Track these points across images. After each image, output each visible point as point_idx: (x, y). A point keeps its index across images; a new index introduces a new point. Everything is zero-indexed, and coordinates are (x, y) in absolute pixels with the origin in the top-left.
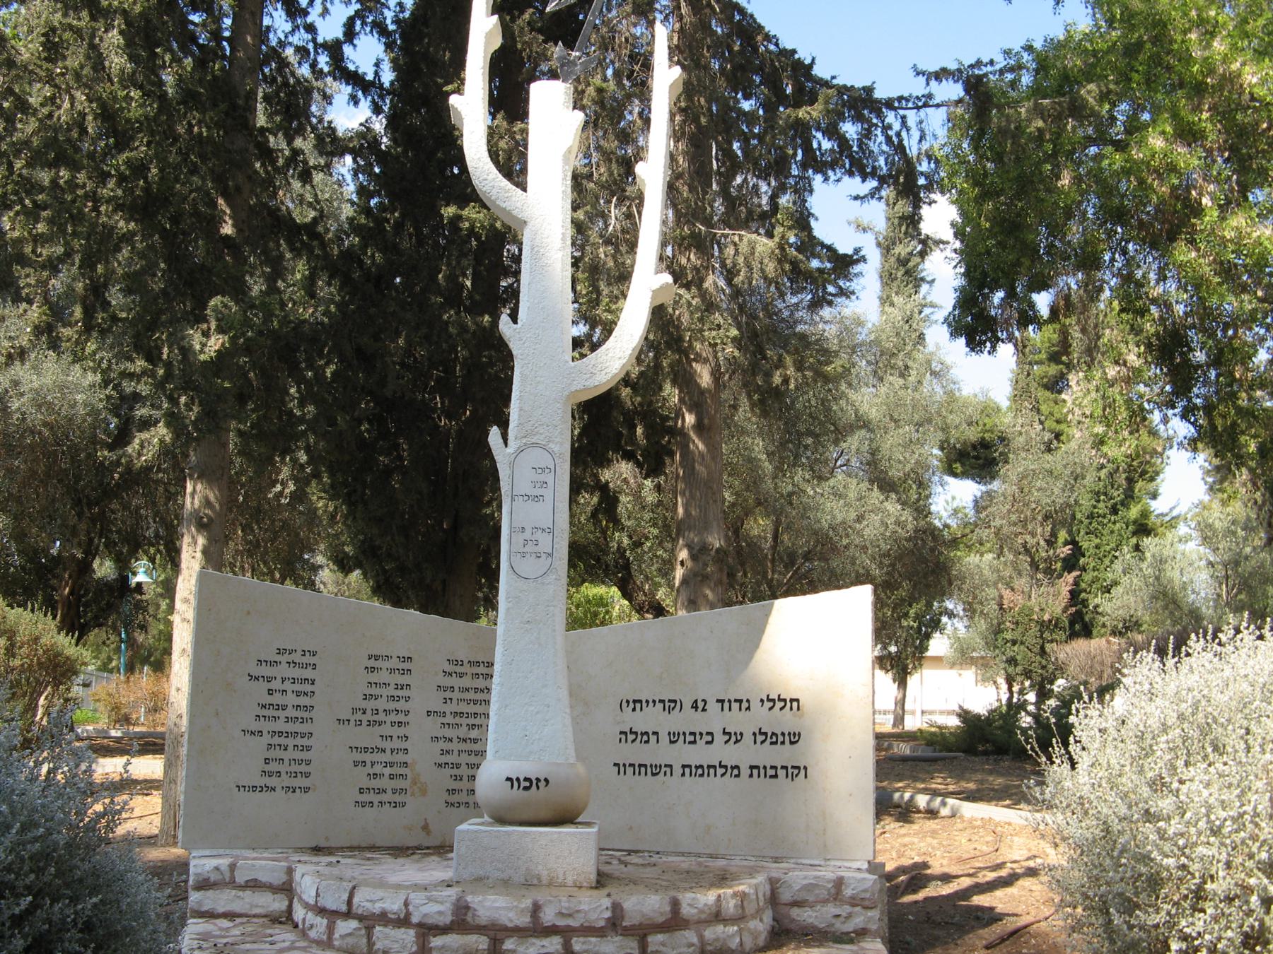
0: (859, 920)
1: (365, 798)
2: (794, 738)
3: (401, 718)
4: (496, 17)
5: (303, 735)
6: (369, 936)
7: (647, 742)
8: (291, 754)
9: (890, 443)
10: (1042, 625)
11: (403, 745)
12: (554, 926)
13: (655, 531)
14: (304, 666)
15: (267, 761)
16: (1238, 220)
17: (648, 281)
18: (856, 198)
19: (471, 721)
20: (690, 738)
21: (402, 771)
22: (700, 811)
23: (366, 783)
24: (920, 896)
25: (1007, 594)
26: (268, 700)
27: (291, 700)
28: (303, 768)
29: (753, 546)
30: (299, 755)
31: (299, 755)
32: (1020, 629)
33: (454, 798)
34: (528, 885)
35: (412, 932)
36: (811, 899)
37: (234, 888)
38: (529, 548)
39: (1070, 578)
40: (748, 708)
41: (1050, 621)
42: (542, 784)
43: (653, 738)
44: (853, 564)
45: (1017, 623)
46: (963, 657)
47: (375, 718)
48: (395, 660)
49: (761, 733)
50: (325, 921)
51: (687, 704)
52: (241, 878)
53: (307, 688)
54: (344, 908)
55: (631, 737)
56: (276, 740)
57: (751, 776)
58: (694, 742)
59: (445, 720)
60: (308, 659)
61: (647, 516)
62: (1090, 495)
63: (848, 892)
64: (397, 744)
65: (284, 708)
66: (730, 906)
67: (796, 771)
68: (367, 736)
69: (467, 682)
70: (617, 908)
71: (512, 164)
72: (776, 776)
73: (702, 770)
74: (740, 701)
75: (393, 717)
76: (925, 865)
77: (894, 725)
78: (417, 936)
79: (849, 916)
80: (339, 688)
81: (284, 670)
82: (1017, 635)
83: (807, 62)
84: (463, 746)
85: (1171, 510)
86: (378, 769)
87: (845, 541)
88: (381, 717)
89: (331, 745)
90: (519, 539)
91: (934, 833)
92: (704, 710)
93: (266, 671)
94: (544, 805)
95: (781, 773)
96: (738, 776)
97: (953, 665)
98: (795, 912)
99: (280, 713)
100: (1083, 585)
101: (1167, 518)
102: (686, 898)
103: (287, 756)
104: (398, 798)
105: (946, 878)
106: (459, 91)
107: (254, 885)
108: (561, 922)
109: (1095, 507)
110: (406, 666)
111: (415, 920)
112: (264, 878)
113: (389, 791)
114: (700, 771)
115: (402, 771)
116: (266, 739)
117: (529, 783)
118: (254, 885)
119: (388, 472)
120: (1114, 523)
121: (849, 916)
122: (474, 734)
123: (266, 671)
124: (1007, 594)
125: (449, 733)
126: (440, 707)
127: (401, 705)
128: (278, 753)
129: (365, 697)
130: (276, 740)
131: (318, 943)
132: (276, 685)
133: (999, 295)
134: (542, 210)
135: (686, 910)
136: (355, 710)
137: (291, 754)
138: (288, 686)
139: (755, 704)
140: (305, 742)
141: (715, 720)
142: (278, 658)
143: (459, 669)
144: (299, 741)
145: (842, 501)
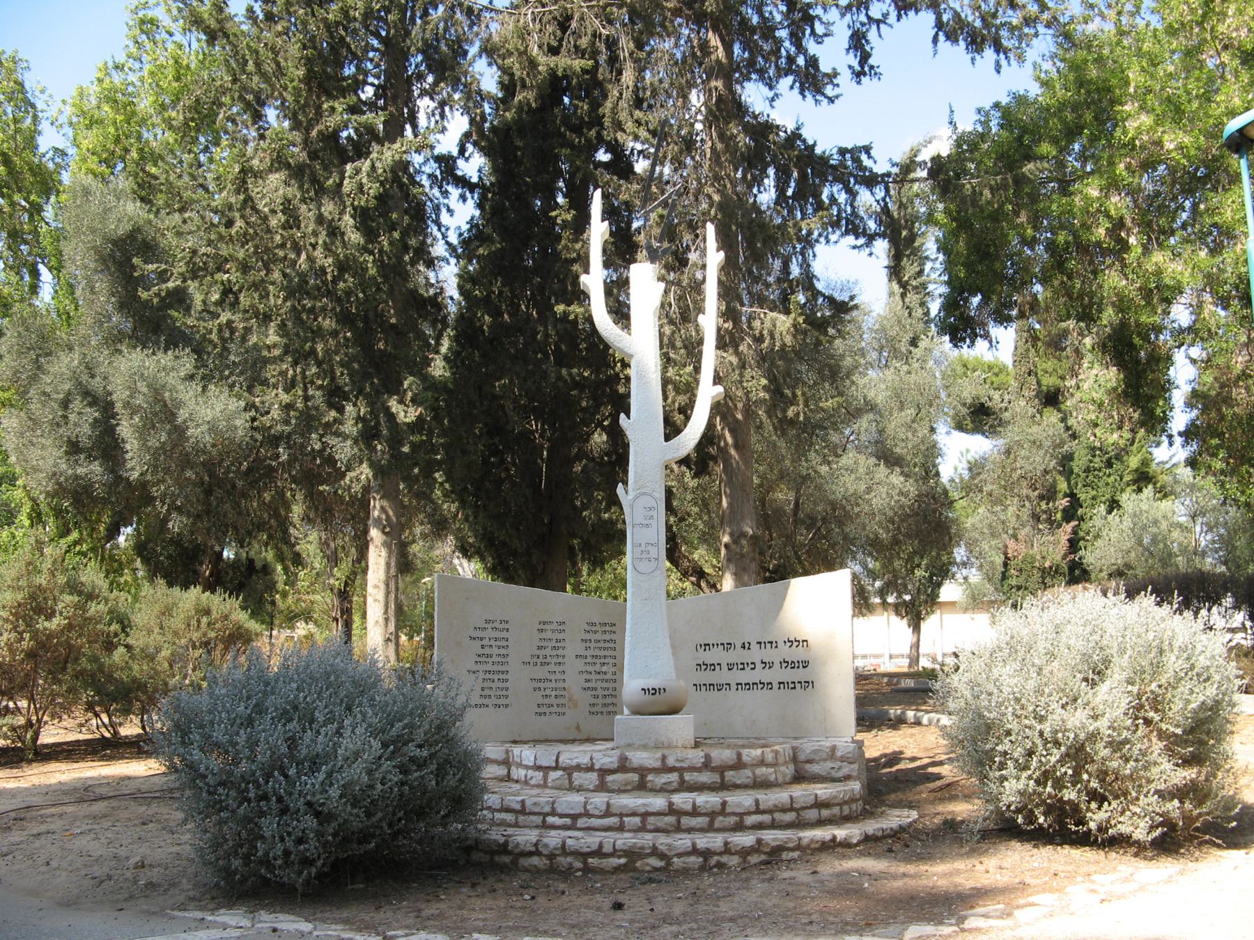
0: (846, 770)
2: (805, 664)
3: (560, 660)
4: (607, 223)
9: (896, 424)
10: (1043, 572)
13: (696, 509)
16: (1158, 257)
18: (854, 247)
19: (603, 660)
22: (749, 711)
23: (541, 701)
24: (894, 769)
25: (1011, 544)
26: (481, 651)
27: (495, 651)
28: (504, 693)
29: (779, 511)
30: (501, 685)
31: (501, 685)
32: (1024, 576)
33: (594, 709)
34: (657, 747)
35: (595, 774)
36: (817, 758)
38: (644, 556)
39: (1068, 528)
41: (1051, 568)
44: (864, 529)
45: (1021, 570)
46: (976, 602)
51: (739, 645)
53: (504, 643)
54: (554, 765)
56: (488, 676)
60: (503, 626)
61: (689, 497)
62: (1086, 451)
63: (839, 754)
64: (558, 676)
66: (770, 757)
67: (808, 684)
68: (540, 672)
69: (599, 636)
70: (707, 757)
71: (621, 313)
73: (749, 686)
76: (901, 753)
77: (910, 666)
79: (840, 768)
82: (1021, 581)
84: (598, 677)
85: (1171, 458)
86: (548, 692)
87: (857, 510)
88: (549, 660)
89: (519, 678)
91: (912, 735)
94: (661, 704)
95: (798, 686)
97: (966, 610)
98: (808, 766)
100: (1081, 534)
101: (1168, 466)
102: (745, 752)
103: (494, 685)
104: (561, 710)
105: (913, 759)
106: (587, 271)
108: (678, 765)
109: (1091, 461)
111: (597, 767)
117: (655, 691)
119: (500, 482)
120: (1109, 475)
121: (840, 768)
124: (1011, 544)
125: (590, 668)
126: (584, 653)
127: (560, 652)
128: (490, 684)
129: (539, 648)
130: (488, 676)
131: (538, 786)
132: (485, 642)
133: (976, 300)
134: (640, 343)
135: (745, 758)
138: (492, 643)
139: (781, 644)
140: (504, 676)
141: (756, 655)
143: (594, 628)
144: (501, 676)
145: (853, 476)
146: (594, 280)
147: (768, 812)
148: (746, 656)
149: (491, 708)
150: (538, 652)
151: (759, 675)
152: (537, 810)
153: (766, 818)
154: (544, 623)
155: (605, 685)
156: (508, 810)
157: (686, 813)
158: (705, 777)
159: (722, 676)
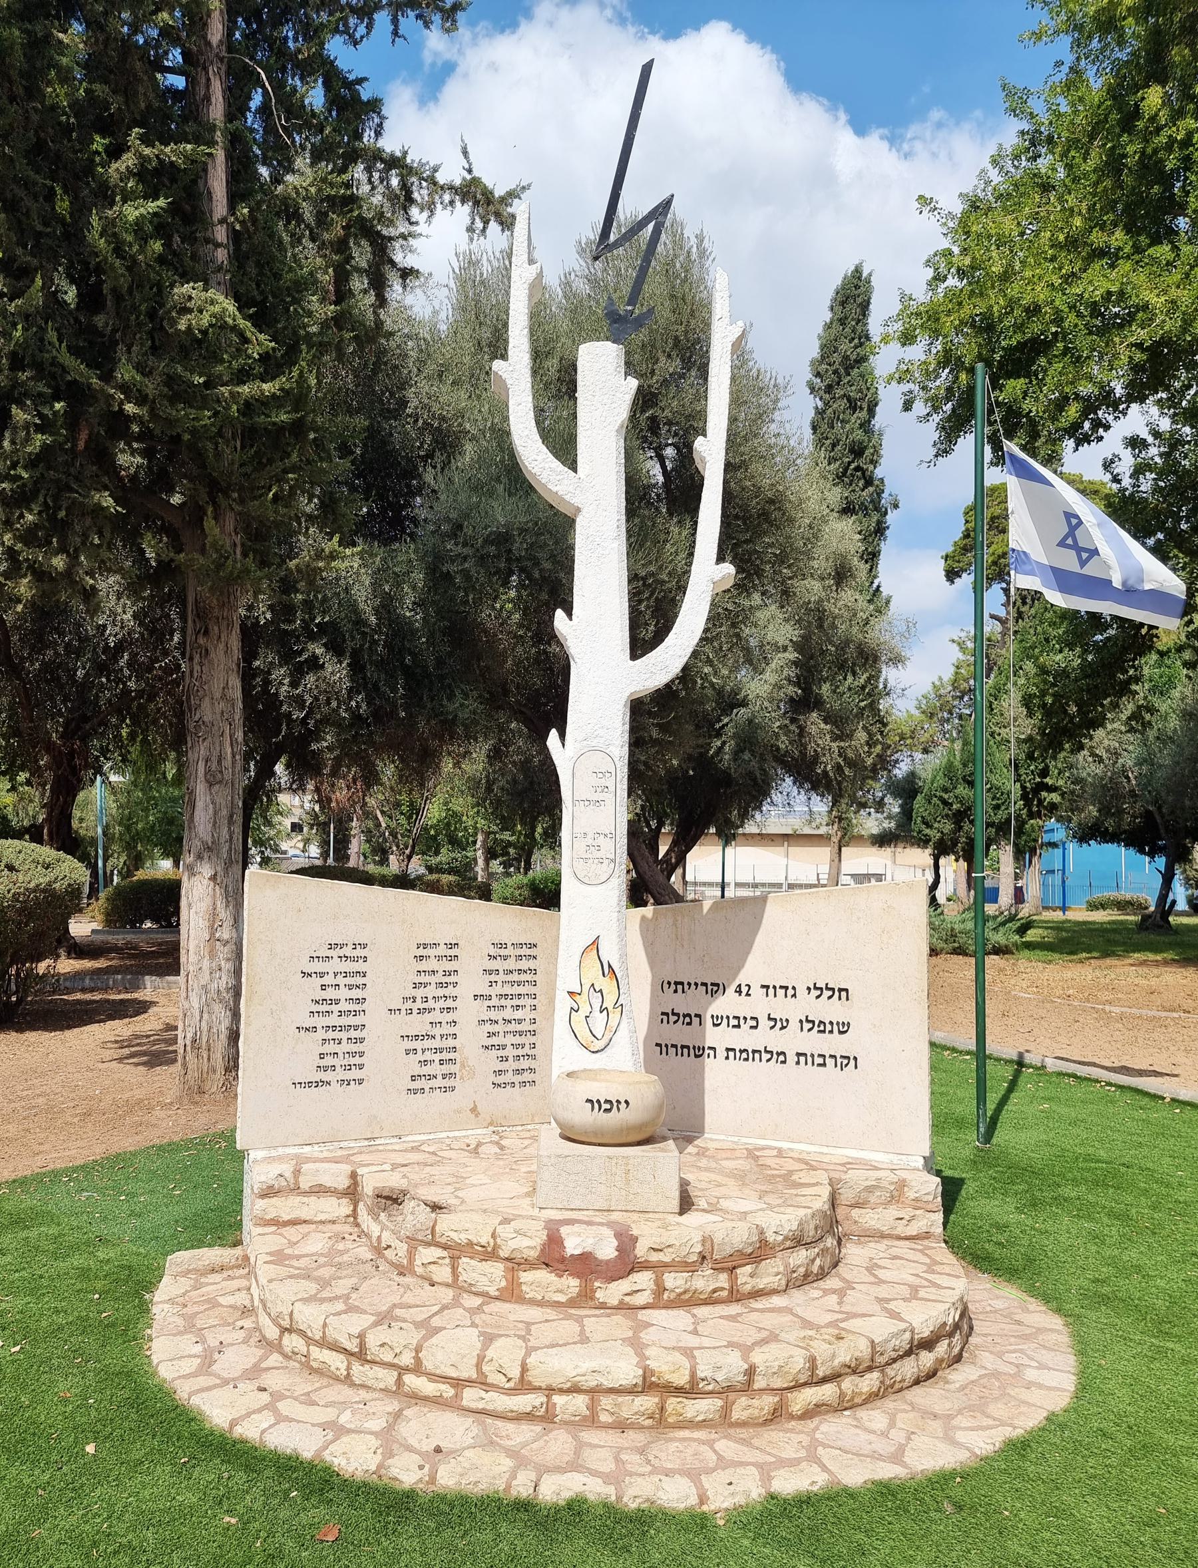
1: (417, 1085)
3: (450, 1003)
5: (356, 1028)
6: (454, 1269)
7: (689, 1024)
8: (346, 1047)
11: (452, 1030)
14: (355, 959)
19: (516, 1002)
20: (734, 1022)
21: (451, 1056)
27: (343, 993)
28: (357, 1060)
35: (500, 1266)
37: (299, 1194)
40: (794, 995)
42: (623, 1105)
43: (696, 1021)
47: (425, 1005)
48: (442, 946)
49: (808, 1021)
52: (305, 1184)
53: (359, 980)
55: (673, 1018)
56: (331, 1035)
57: (798, 1063)
58: (738, 1026)
59: (491, 1003)
60: (359, 952)
64: (446, 1030)
65: (337, 1002)
68: (418, 1024)
69: (511, 964)
71: (564, 446)
72: (824, 1065)
73: (746, 1055)
74: (786, 988)
75: (442, 1004)
78: (506, 1269)
79: (913, 1218)
80: (389, 979)
81: (337, 965)
83: (398, 154)
86: (428, 1056)
90: (580, 845)
92: (748, 995)
93: (318, 967)
96: (784, 1062)
99: (334, 1008)
104: (447, 1083)
107: (320, 1190)
108: (655, 1257)
112: (328, 1182)
113: (440, 1077)
114: (744, 1055)
115: (451, 1056)
116: (321, 1034)
117: (610, 1106)
118: (320, 1190)
121: (913, 1218)
123: (318, 967)
125: (493, 1015)
126: (486, 992)
127: (449, 991)
128: (330, 1048)
132: (329, 980)
136: (405, 999)
137: (346, 1047)
138: (340, 980)
139: (801, 991)
142: (330, 953)
143: (503, 952)
144: (353, 1034)
147: (833, 1377)
150: (414, 993)
152: (388, 1357)
153: (827, 1392)
154: (425, 946)
155: (518, 1040)
156: (336, 1348)
157: (679, 1391)
158: (706, 1281)
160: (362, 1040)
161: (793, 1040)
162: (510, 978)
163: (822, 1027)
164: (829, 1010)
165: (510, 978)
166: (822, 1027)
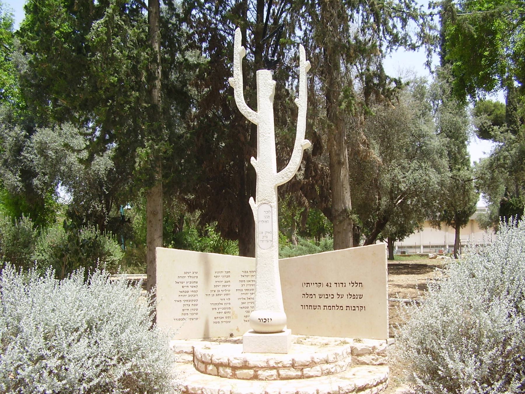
1: (217, 320)
3: (227, 292)
5: (195, 301)
8: (191, 307)
11: (229, 302)
12: (274, 366)
14: (193, 277)
15: (183, 310)
17: (302, 143)
21: (229, 310)
26: (182, 290)
27: (190, 289)
28: (196, 312)
42: (270, 320)
47: (219, 293)
50: (204, 365)
51: (325, 285)
53: (195, 284)
56: (186, 303)
59: (242, 292)
60: (195, 275)
65: (188, 292)
68: (217, 300)
69: (249, 278)
75: (225, 292)
79: (377, 359)
81: (187, 279)
84: (249, 301)
86: (221, 310)
88: (221, 293)
95: (357, 308)
99: (186, 294)
103: (189, 308)
104: (228, 320)
110: (228, 274)
115: (229, 310)
116: (183, 303)
122: (252, 296)
126: (240, 288)
127: (227, 288)
128: (187, 307)
130: (186, 303)
132: (184, 284)
136: (212, 291)
137: (191, 307)
138: (188, 284)
139: (347, 284)
140: (195, 303)
141: (334, 290)
142: (185, 275)
143: (246, 274)
144: (194, 303)
146: (237, 81)
148: (329, 291)
149: (188, 320)
151: (336, 301)
158: (293, 373)
159: (316, 301)
160: (197, 305)
161: (345, 302)
162: (249, 283)
163: (354, 297)
164: (356, 290)
165: (249, 283)
166: (354, 297)
